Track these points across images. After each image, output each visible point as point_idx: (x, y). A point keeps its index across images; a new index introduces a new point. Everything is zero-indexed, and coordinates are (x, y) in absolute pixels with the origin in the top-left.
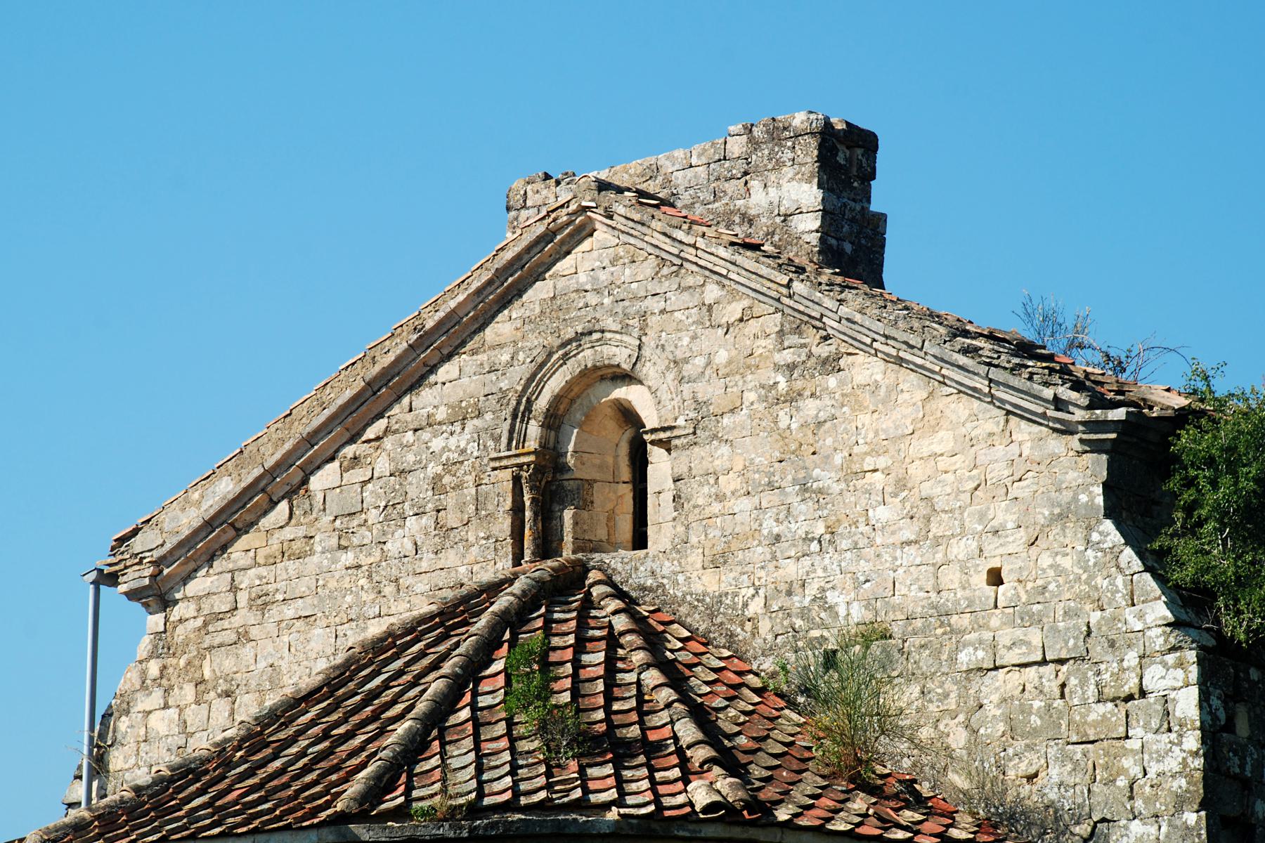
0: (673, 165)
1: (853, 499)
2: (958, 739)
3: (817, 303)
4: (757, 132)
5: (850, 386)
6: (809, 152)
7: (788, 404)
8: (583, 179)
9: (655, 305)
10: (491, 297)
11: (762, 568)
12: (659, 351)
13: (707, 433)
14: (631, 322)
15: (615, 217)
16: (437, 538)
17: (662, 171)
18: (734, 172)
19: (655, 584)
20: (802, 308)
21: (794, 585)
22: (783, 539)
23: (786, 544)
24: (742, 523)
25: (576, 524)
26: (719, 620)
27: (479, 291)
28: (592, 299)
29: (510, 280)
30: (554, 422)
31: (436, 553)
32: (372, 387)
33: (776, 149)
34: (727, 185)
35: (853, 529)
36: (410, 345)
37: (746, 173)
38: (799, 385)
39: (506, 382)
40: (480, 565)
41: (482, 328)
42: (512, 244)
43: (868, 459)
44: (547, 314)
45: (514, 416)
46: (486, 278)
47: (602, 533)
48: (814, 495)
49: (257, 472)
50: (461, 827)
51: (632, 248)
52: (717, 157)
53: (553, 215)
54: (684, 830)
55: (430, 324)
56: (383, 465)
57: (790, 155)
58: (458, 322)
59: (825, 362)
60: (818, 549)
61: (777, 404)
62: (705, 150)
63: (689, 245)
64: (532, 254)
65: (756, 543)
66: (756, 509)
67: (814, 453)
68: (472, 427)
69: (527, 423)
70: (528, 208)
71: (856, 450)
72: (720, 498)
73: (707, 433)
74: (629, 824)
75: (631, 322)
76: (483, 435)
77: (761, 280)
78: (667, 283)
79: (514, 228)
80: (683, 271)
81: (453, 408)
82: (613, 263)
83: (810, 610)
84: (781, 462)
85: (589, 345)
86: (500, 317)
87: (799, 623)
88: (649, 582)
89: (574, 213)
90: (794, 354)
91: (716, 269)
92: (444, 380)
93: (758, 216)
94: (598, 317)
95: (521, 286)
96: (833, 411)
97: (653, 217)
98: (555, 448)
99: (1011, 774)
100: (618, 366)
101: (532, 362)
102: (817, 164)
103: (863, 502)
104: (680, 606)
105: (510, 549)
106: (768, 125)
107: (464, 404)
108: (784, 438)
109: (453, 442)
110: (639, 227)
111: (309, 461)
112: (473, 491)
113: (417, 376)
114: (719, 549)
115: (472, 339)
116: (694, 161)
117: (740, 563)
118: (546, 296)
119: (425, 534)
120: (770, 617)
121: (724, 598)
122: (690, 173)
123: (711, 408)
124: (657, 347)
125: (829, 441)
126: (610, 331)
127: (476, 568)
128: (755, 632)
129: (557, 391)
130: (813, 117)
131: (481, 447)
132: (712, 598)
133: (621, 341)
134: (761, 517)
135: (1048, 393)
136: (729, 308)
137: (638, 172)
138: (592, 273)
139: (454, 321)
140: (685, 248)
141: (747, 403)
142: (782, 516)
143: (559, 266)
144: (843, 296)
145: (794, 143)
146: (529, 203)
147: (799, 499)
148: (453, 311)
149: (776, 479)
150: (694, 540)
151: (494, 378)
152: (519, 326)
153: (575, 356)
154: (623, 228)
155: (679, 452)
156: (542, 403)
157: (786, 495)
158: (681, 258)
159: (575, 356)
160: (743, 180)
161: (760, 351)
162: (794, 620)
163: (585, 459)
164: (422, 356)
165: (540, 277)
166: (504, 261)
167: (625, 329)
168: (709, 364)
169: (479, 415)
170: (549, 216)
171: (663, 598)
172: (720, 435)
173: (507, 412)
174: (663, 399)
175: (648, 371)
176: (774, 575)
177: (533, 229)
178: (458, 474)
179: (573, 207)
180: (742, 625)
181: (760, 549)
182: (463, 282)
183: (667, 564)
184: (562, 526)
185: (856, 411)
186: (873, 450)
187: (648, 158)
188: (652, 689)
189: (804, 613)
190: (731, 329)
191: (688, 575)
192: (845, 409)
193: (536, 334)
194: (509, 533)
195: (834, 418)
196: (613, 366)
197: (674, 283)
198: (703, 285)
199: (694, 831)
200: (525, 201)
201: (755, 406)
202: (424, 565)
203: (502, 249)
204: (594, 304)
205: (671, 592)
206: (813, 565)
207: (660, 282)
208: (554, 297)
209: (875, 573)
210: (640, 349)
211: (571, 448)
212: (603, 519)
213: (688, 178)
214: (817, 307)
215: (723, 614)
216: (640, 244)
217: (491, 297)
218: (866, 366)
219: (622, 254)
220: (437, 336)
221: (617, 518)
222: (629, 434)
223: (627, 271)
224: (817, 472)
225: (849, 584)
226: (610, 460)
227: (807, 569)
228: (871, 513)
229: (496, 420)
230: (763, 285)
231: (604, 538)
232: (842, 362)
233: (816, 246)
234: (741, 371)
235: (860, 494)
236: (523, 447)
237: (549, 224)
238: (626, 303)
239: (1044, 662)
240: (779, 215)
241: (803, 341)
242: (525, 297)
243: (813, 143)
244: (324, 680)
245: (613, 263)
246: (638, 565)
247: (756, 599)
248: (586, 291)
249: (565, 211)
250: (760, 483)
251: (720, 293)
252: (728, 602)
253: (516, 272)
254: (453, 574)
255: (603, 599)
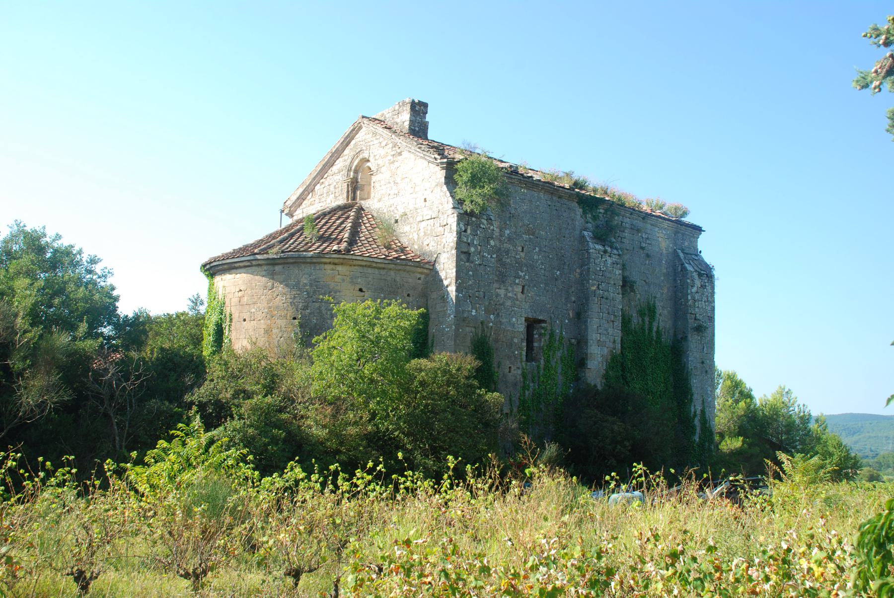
2: (416, 237)
4: (401, 104)
6: (408, 107)
32: (324, 166)
47: (366, 196)
49: (305, 186)
56: (327, 184)
59: (399, 153)
99: (424, 244)
111: (315, 183)
135: (433, 156)
156: (353, 168)
165: (353, 139)
173: (347, 170)
175: (371, 159)
189: (393, 211)
197: (374, 138)
212: (367, 193)
229: (345, 172)
239: (431, 219)
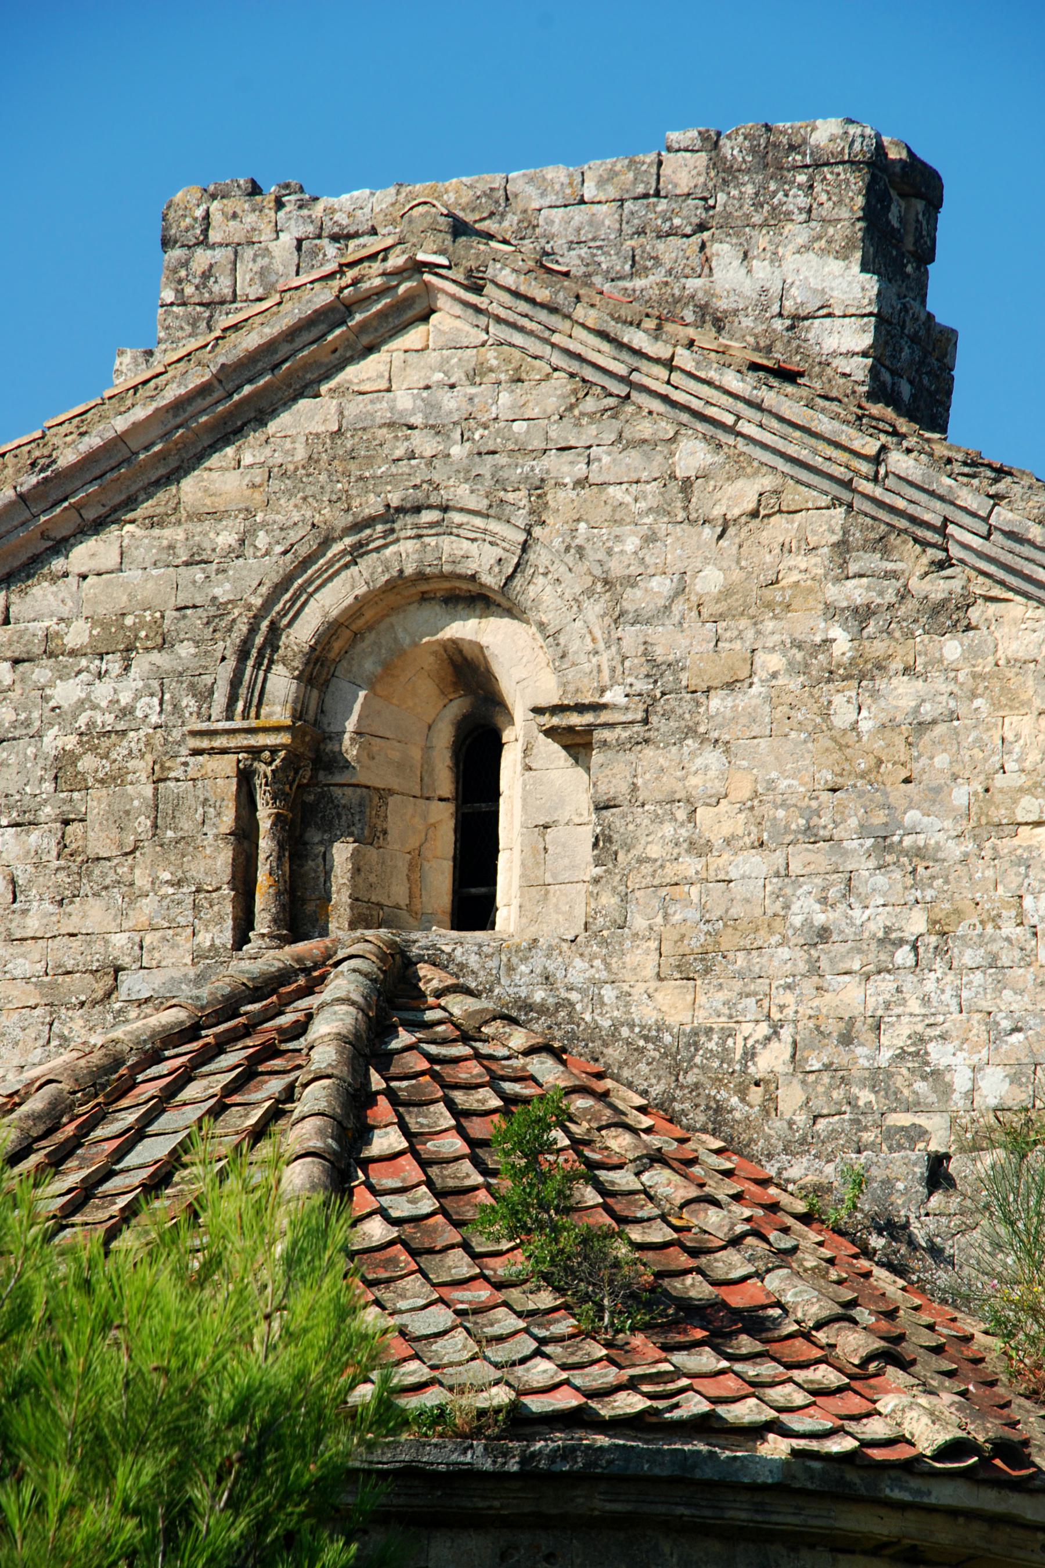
0: (543, 195)
1: (990, 873)
3: (941, 498)
4: (730, 149)
5: (991, 659)
7: (855, 683)
8: (421, 209)
9: (566, 469)
10: (203, 419)
11: (788, 987)
12: (570, 558)
13: (673, 724)
14: (510, 497)
15: (489, 289)
16: (62, 875)
17: (518, 205)
18: (677, 221)
19: (551, 1000)
20: (901, 504)
21: (858, 1024)
22: (835, 937)
23: (843, 948)
24: (748, 901)
25: (357, 870)
26: (691, 1078)
27: (178, 405)
28: (426, 444)
29: (247, 389)
30: (319, 673)
31: (61, 903)
33: (773, 186)
34: (661, 246)
35: (990, 929)
36: (21, 496)
37: (702, 227)
38: (878, 648)
39: (227, 586)
40: (159, 934)
41: (174, 476)
42: (258, 320)
43: (1026, 801)
44: (323, 464)
45: (243, 655)
46: (199, 381)
47: (398, 892)
48: (904, 860)
50: (506, 1454)
51: (517, 354)
52: (640, 189)
53: (351, 274)
54: (902, 1489)
55: (67, 458)
57: (803, 201)
58: (128, 460)
59: (937, 609)
60: (910, 960)
61: (829, 681)
62: (613, 174)
63: (657, 361)
64: (298, 343)
65: (775, 939)
66: (777, 875)
67: (907, 781)
68: (146, 667)
69: (268, 670)
70: (212, 247)
71: (1000, 781)
72: (699, 848)
73: (673, 724)
74: (808, 1469)
75: (510, 497)
76: (171, 684)
77: (813, 441)
78: (593, 429)
79: (180, 281)
80: (630, 409)
81: (104, 625)
82: (475, 375)
83: (890, 1075)
84: (834, 790)
85: (410, 533)
86: (214, 460)
87: (865, 1096)
88: (539, 996)
89: (399, 273)
90: (868, 588)
91: (711, 412)
92: (84, 570)
93: (736, 312)
94: (436, 478)
95: (264, 404)
96: (952, 704)
97: (578, 297)
98: (316, 723)
100: (473, 578)
101: (285, 552)
102: (860, 225)
103: (1013, 880)
104: (606, 1045)
105: (229, 908)
106: (754, 138)
107: (129, 621)
108: (841, 747)
109: (103, 691)
110: (543, 315)
112: (148, 791)
113: (23, 557)
114: (694, 944)
115: (150, 496)
116: (589, 191)
117: (740, 975)
118: (321, 429)
119: (36, 865)
120: (803, 1082)
121: (703, 1039)
122: (579, 215)
123: (684, 677)
124: (567, 549)
125: (942, 760)
126: (462, 510)
127: (149, 939)
128: (770, 1106)
129: (335, 613)
130: (853, 130)
131: (168, 708)
132: (677, 1037)
133: (485, 531)
134: (788, 891)
136: (731, 489)
137: (463, 201)
138: (425, 394)
139: (119, 457)
140: (644, 365)
141: (761, 674)
142: (833, 894)
143: (351, 373)
144: (1001, 487)
145: (811, 178)
146: (214, 236)
147: (872, 863)
148: (120, 438)
149: (823, 822)
150: (639, 922)
151: (200, 576)
152: (258, 480)
153: (377, 549)
154: (503, 313)
155: (610, 754)
157: (845, 853)
158: (631, 384)
159: (377, 549)
160: (696, 240)
161: (795, 577)
162: (855, 1090)
163: (375, 749)
164: (43, 519)
166: (239, 353)
167: (496, 510)
168: (681, 590)
169: (164, 644)
170: (343, 273)
171: (569, 1027)
172: (702, 729)
174: (573, 648)
176: (815, 1003)
177: (306, 294)
178: (113, 755)
179: (396, 260)
180: (742, 1092)
181: (784, 953)
182: (145, 383)
183: (578, 962)
184: (328, 874)
185: (1001, 707)
186: (1036, 785)
187: (487, 177)
188: (682, 1207)
189: (877, 1079)
190: (732, 531)
191: (626, 987)
192: (978, 702)
193: (297, 499)
194: (227, 878)
195: (953, 716)
196: (459, 577)
198: (673, 440)
199: (919, 1492)
200: (205, 231)
201: (780, 681)
202: (33, 924)
203: (236, 327)
204: (428, 453)
205: (587, 1017)
206: (898, 990)
207: (578, 425)
208: (339, 432)
209: (1035, 1016)
210: (524, 550)
211: (351, 725)
212: (402, 864)
213: (575, 223)
214: (938, 505)
215: (702, 1067)
216: (535, 347)
217: (203, 419)
218: (1029, 624)
219: (494, 363)
220: (78, 483)
221: (426, 866)
222: (458, 707)
223: (505, 398)
224: (912, 816)
225: (978, 1029)
226: (416, 754)
227: (887, 996)
228: (1028, 902)
230: (815, 452)
231: (403, 902)
232: (974, 614)
233: (863, 383)
234: (752, 611)
235: (1006, 865)
236: (258, 717)
237: (341, 290)
238: (502, 459)
240: (780, 315)
241: (890, 566)
242: (272, 427)
243: (855, 184)
244: (21, 1140)
245: (475, 375)
246: (515, 960)
247: (774, 1044)
248: (411, 427)
249: (377, 267)
250: (787, 827)
251: (710, 459)
252: (712, 1045)
253: (261, 374)
254: (99, 946)
255: (486, 1023)
